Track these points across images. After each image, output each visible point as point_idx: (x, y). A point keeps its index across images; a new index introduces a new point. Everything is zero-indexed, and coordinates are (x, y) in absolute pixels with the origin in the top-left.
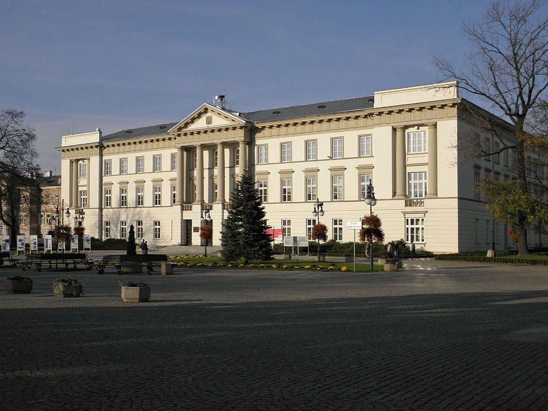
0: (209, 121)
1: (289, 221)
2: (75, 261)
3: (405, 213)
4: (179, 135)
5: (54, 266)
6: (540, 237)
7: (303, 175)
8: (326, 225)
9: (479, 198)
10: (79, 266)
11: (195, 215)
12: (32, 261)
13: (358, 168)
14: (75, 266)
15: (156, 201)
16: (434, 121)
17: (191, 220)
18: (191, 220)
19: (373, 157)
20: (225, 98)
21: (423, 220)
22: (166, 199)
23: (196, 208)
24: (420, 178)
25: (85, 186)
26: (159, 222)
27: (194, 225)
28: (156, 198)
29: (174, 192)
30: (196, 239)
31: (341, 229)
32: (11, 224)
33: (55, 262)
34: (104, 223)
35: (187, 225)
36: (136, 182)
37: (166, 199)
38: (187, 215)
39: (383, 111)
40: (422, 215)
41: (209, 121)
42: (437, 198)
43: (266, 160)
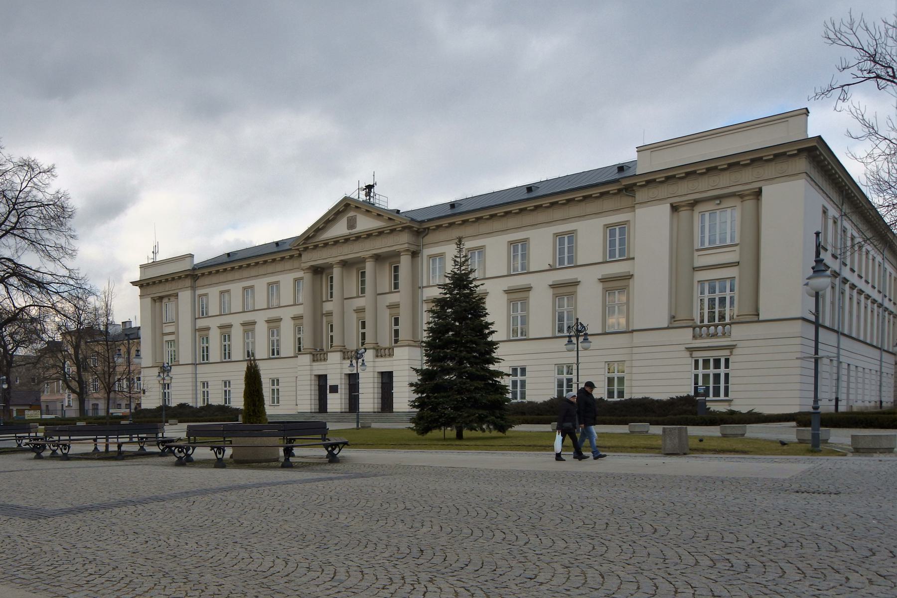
0: (351, 224)
1: (523, 370)
2: (142, 438)
3: (691, 350)
4: (306, 249)
5: (102, 448)
6: (816, 400)
7: (291, 323)
8: (183, 402)
9: (841, 321)
10: (148, 449)
11: (335, 369)
12: (59, 440)
13: (268, 321)
14: (142, 447)
15: (273, 350)
16: (756, 185)
17: (391, 373)
18: (391, 373)
19: (633, 258)
20: (376, 189)
21: (727, 361)
22: (287, 347)
23: (334, 358)
24: (723, 290)
25: (172, 333)
26: (278, 380)
27: (330, 382)
28: (273, 345)
29: (298, 336)
30: (336, 402)
31: (523, 383)
32: (78, 390)
33: (128, 440)
34: (199, 384)
35: (322, 386)
36: (220, 327)
37: (287, 347)
38: (320, 368)
39: (738, 160)
40: (726, 353)
41: (351, 224)
42: (759, 321)
43: (571, 260)
